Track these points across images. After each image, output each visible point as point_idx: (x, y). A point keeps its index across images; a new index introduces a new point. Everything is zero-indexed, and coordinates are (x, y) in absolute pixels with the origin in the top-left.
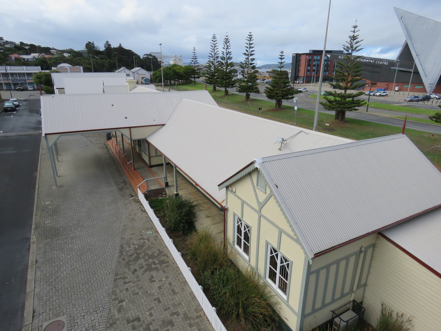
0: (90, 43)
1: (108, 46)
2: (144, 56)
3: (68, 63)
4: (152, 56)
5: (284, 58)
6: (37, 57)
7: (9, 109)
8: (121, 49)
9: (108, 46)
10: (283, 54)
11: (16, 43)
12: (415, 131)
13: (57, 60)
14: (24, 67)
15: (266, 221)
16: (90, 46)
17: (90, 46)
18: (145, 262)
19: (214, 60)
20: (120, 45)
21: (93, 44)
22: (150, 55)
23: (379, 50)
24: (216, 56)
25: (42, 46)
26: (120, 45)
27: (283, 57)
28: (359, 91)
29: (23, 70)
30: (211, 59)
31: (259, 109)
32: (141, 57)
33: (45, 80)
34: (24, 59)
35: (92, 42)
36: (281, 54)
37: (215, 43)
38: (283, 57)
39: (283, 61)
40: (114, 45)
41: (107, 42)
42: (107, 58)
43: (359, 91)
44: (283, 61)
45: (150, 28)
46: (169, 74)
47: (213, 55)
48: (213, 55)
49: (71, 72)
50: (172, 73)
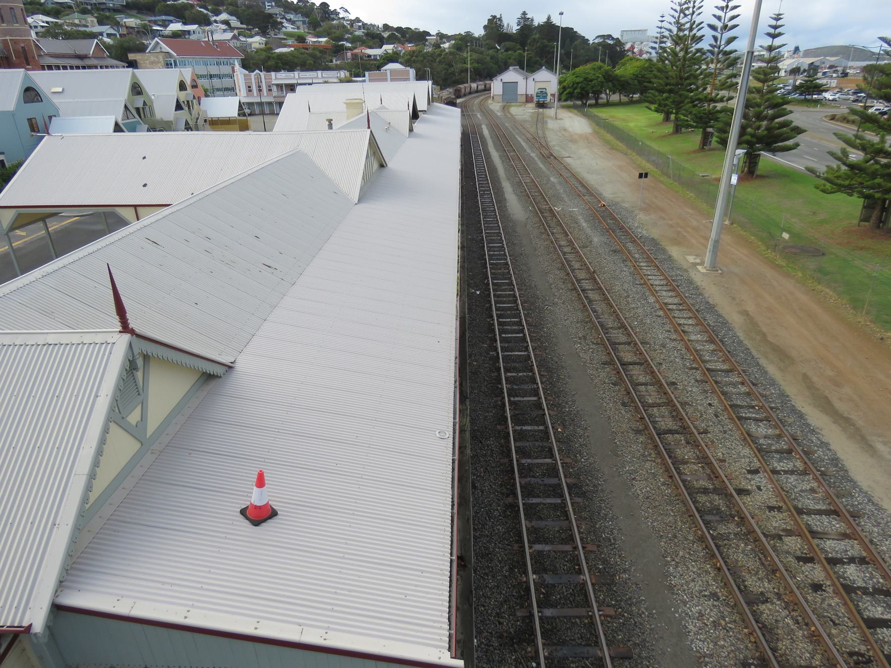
0: (494, 17)
2: (596, 41)
4: (613, 39)
5: (780, 34)
6: (390, 51)
8: (549, 28)
10: (779, 23)
12: (499, 191)
15: (128, 316)
16: (494, 25)
17: (494, 25)
20: (549, 18)
21: (500, 19)
23: (193, 37)
26: (549, 18)
27: (778, 31)
29: (317, 78)
31: (641, 176)
32: (591, 42)
34: (369, 56)
35: (498, 16)
36: (774, 23)
38: (778, 31)
39: (777, 42)
40: (539, 19)
41: (524, 13)
44: (777, 42)
46: (591, 81)
49: (392, 80)
50: (601, 79)
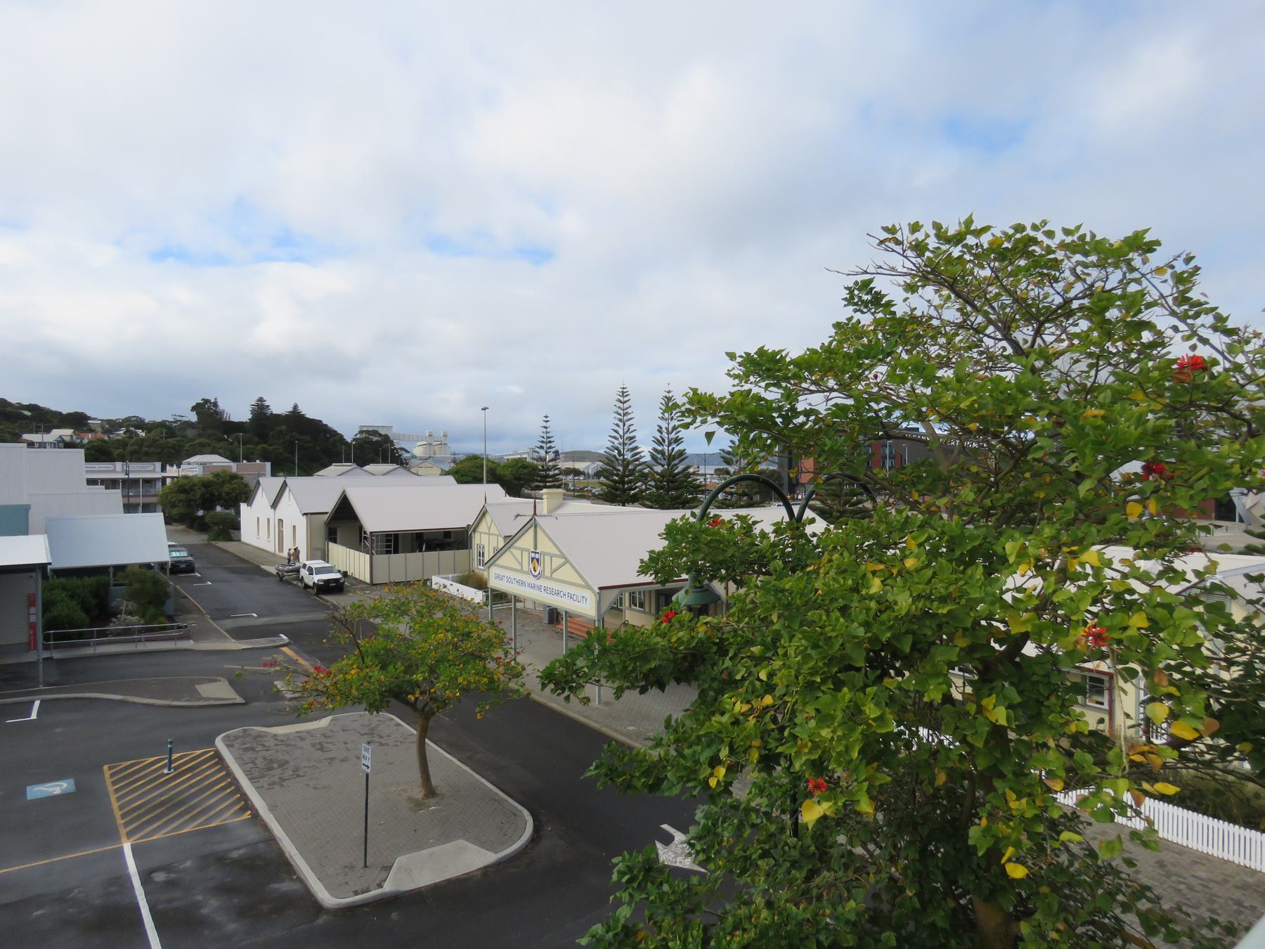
0: (206, 401)
1: (260, 410)
3: (220, 454)
4: (380, 435)
7: (183, 566)
8: (296, 419)
9: (260, 410)
11: (717, 396)
13: (141, 446)
14: (119, 465)
18: (35, 648)
19: (624, 444)
20: (296, 407)
21: (215, 404)
22: (375, 433)
24: (628, 435)
25: (64, 412)
26: (296, 407)
28: (234, 467)
29: (114, 471)
30: (616, 442)
33: (203, 495)
37: (626, 405)
40: (279, 406)
41: (261, 400)
42: (256, 439)
43: (234, 467)
45: (339, 368)
47: (621, 433)
48: (621, 433)
